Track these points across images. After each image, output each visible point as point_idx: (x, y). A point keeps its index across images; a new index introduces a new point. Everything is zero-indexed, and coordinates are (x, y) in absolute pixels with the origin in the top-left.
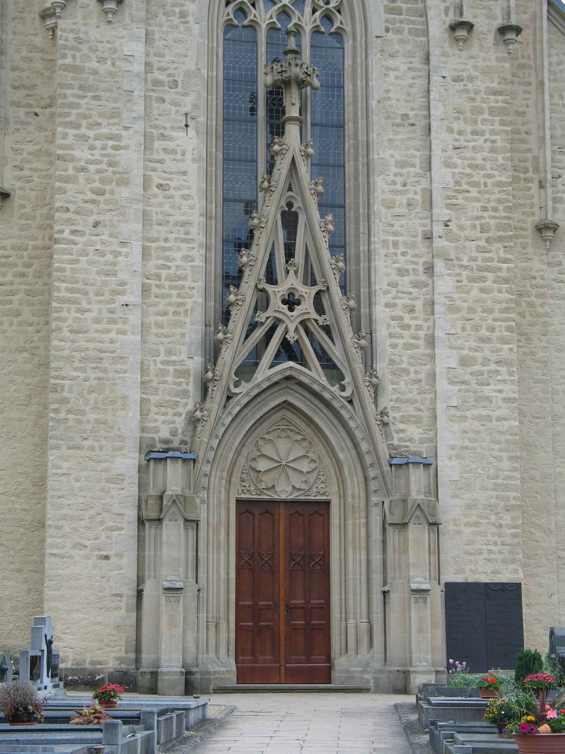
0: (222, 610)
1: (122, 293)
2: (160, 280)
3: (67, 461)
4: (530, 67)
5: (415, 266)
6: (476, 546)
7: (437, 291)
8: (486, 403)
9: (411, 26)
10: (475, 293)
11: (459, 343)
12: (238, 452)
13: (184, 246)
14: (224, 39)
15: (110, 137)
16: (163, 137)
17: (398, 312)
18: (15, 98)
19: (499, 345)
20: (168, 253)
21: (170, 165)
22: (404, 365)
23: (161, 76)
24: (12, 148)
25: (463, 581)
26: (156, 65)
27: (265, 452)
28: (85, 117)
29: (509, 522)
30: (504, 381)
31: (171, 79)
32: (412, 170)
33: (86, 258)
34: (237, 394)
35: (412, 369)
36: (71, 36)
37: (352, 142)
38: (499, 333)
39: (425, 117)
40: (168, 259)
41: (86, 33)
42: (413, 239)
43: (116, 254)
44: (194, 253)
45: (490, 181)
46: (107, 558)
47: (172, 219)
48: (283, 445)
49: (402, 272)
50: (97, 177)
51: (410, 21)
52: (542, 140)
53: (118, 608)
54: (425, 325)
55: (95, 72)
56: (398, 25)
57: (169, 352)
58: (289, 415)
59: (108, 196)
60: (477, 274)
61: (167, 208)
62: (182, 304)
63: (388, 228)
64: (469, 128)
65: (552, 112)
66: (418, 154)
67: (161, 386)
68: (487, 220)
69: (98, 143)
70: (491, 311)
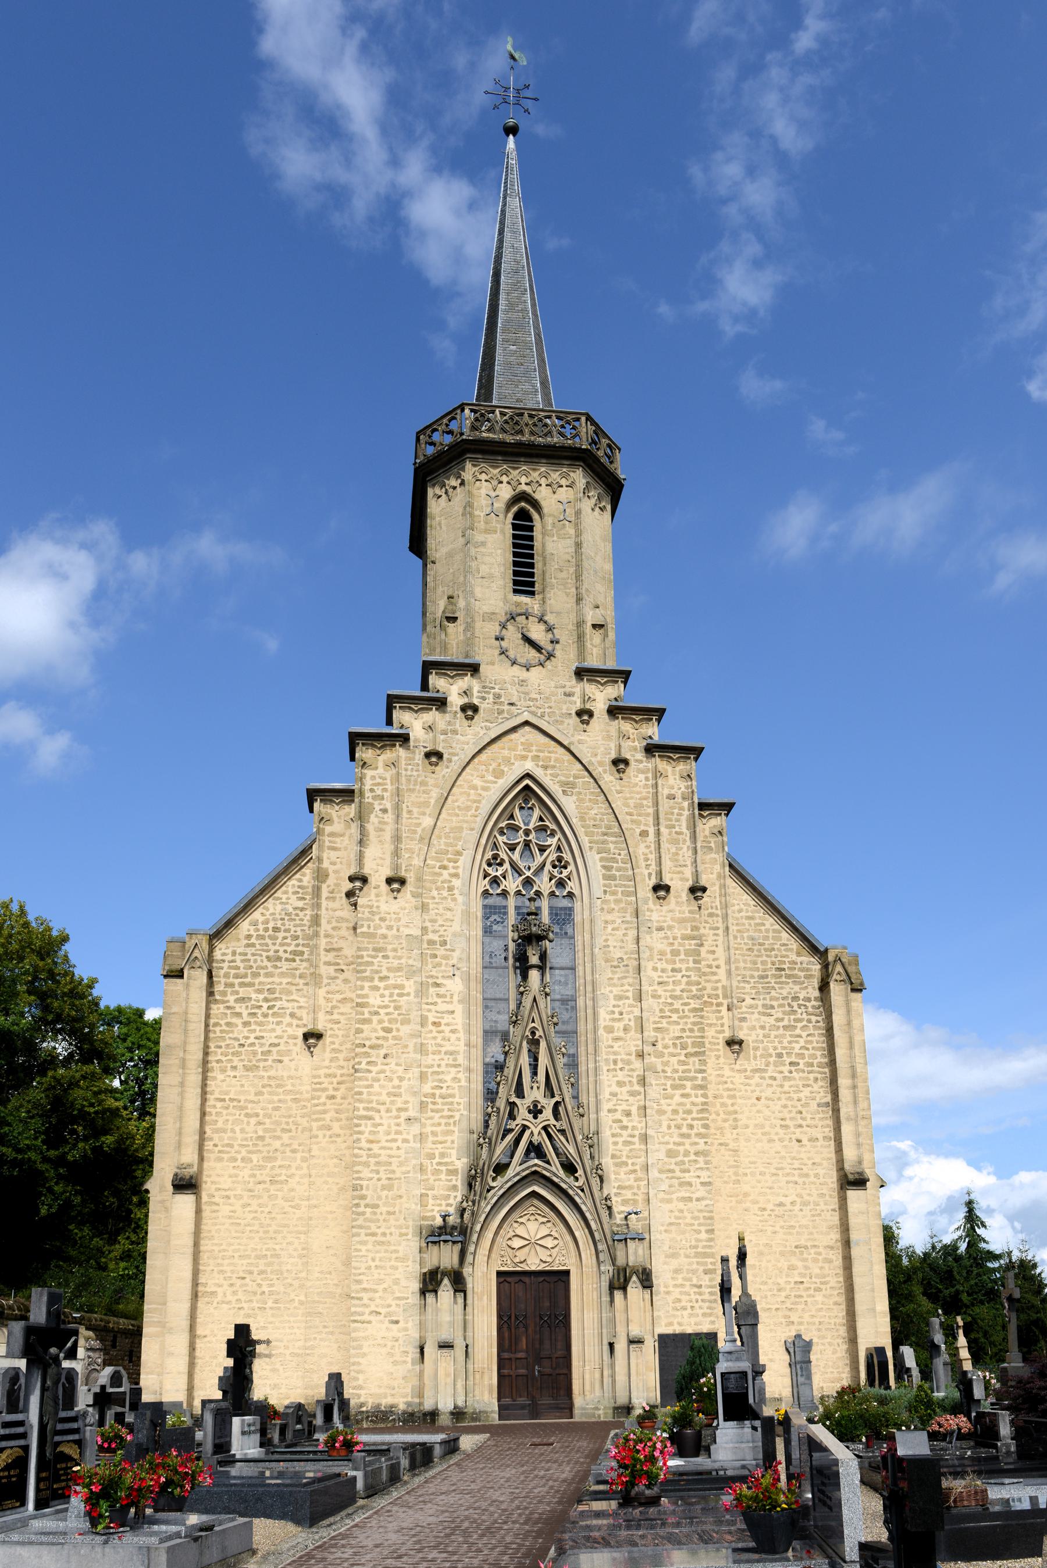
1: (406, 1110)
6: (683, 1304)
10: (677, 1099)
11: (667, 1138)
13: (453, 1070)
15: (395, 987)
16: (437, 985)
17: (618, 1116)
18: (327, 959)
19: (697, 1140)
20: (441, 1077)
22: (624, 1159)
23: (436, 938)
26: (430, 929)
27: (518, 1232)
35: (630, 1162)
40: (441, 1081)
44: (460, 1075)
45: (686, 1008)
46: (397, 1322)
47: (443, 1049)
48: (532, 1226)
49: (620, 1084)
50: (386, 1018)
53: (405, 1362)
55: (385, 937)
58: (536, 1202)
59: (394, 1033)
60: (678, 1082)
61: (439, 1041)
64: (670, 967)
69: (387, 993)
70: (689, 1112)
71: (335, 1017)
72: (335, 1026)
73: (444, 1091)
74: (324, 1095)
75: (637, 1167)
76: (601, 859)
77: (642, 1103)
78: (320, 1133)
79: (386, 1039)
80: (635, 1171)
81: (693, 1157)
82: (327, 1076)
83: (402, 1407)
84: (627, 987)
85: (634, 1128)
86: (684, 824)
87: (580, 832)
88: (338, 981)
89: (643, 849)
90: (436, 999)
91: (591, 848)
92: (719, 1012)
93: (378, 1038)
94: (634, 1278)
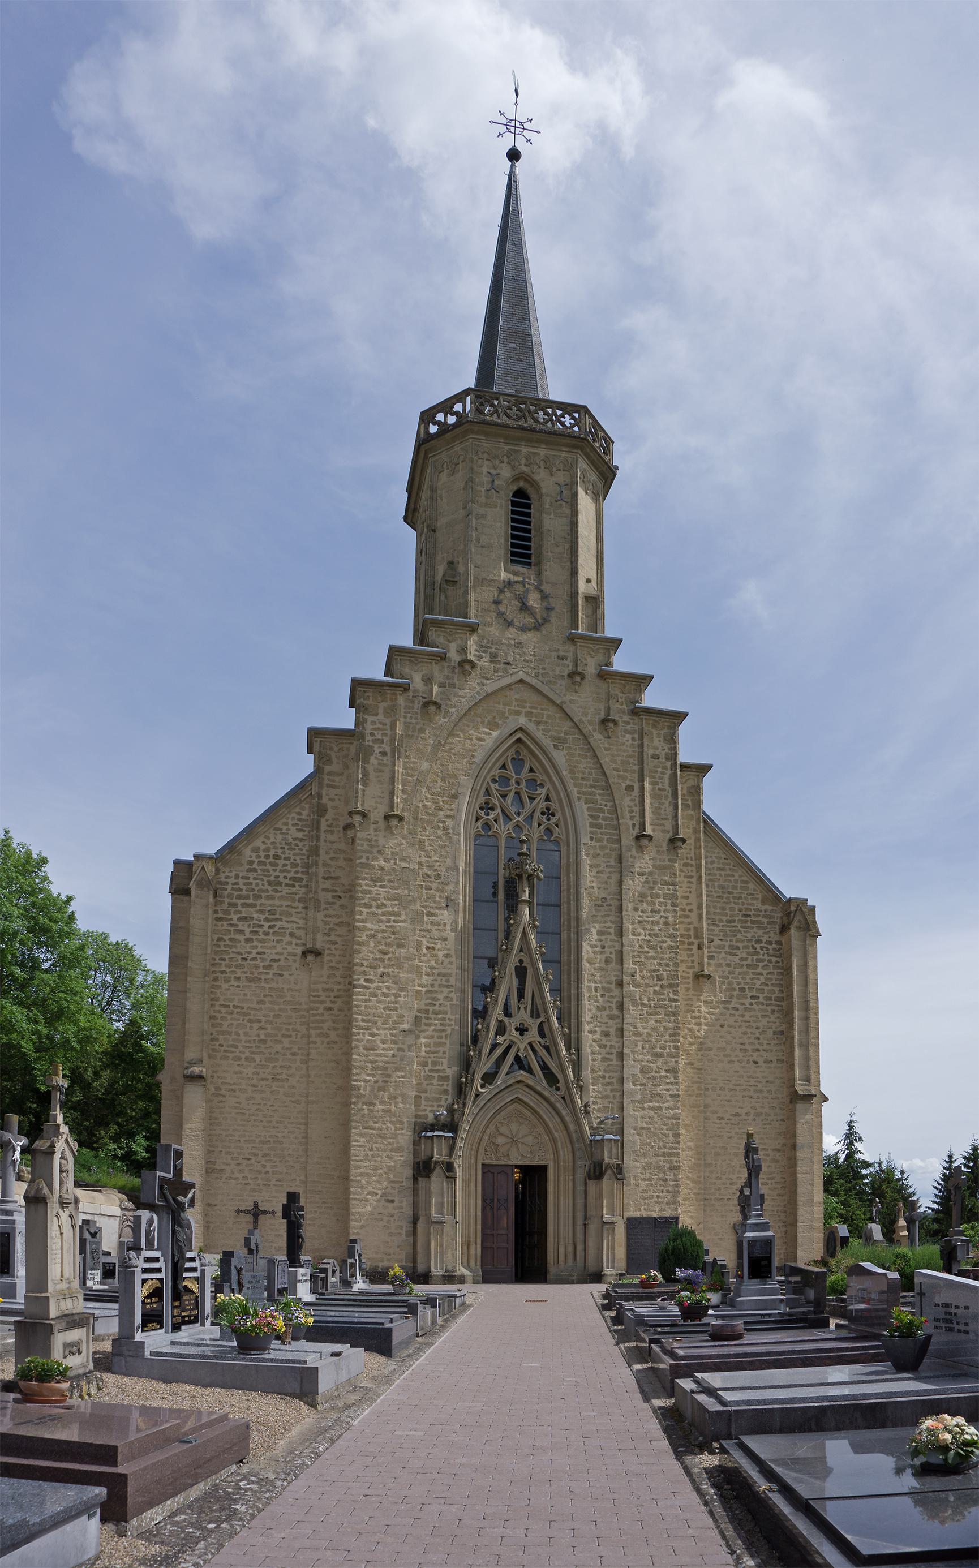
4: (692, 866)
7: (626, 1021)
13: (446, 990)
15: (394, 914)
17: (597, 1036)
18: (325, 886)
21: (436, 934)
28: (375, 900)
29: (672, 1177)
30: (671, 1083)
35: (607, 1075)
40: (434, 999)
41: (376, 841)
43: (396, 996)
46: (392, 1201)
52: (700, 916)
54: (617, 1045)
55: (382, 869)
57: (435, 1063)
65: (707, 896)
67: (429, 1087)
71: (333, 938)
72: (333, 947)
73: (437, 1008)
74: (322, 1007)
75: (614, 1080)
76: (588, 809)
77: (619, 1026)
78: (318, 1040)
79: (382, 960)
80: (611, 1083)
81: (664, 1074)
82: (324, 990)
84: (609, 924)
86: (667, 782)
88: (336, 907)
90: (429, 927)
91: (579, 799)
92: (691, 950)
93: (376, 959)
94: (609, 1172)
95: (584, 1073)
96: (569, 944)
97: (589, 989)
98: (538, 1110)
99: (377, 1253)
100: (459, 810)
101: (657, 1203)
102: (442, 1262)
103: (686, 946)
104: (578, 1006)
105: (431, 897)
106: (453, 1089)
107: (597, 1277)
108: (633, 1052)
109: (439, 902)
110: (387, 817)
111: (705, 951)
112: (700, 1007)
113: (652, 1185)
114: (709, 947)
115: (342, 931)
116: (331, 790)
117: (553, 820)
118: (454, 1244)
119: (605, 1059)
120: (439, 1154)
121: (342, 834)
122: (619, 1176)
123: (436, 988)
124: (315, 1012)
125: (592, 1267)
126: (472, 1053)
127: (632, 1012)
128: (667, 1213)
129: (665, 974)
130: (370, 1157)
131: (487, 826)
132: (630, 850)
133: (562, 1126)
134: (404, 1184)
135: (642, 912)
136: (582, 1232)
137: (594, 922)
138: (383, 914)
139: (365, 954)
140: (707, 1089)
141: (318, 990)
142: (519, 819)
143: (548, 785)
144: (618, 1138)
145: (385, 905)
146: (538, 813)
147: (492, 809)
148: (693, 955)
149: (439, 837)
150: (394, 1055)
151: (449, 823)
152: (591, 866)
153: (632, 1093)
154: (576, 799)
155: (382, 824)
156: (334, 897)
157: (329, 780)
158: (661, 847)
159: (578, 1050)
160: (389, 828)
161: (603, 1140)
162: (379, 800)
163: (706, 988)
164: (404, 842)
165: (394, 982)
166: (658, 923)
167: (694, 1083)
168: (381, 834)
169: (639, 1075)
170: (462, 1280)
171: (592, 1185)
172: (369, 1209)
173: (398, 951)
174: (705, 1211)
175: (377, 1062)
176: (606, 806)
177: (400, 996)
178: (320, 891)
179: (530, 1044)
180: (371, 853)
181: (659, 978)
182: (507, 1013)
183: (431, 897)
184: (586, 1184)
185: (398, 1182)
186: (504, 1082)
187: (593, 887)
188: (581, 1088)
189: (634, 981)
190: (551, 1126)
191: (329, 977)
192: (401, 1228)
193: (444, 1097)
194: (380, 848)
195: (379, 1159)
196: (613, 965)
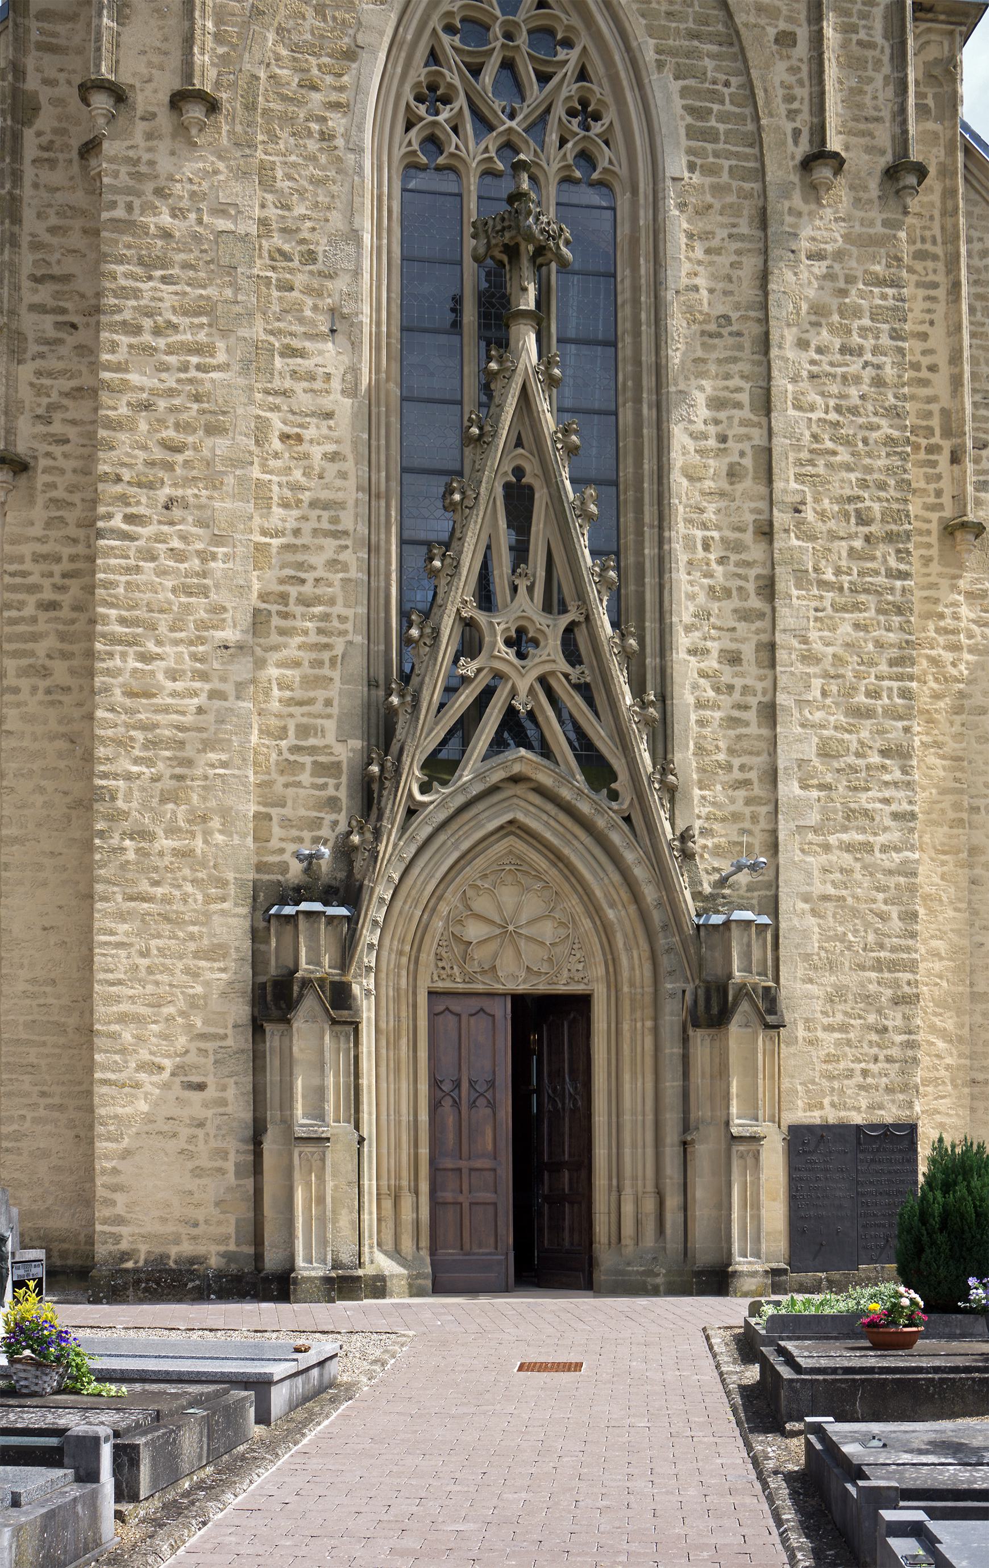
0: (405, 1174)
2: (286, 605)
3: (125, 921)
4: (935, 257)
5: (742, 583)
7: (780, 625)
8: (863, 822)
9: (734, 162)
11: (818, 716)
12: (431, 909)
13: (331, 544)
14: (404, 190)
15: (197, 350)
17: (712, 663)
18: (36, 299)
20: (300, 557)
21: (304, 401)
24: (31, 384)
25: (818, 1121)
28: (149, 314)
29: (899, 1022)
30: (895, 784)
31: (304, 248)
32: (737, 413)
33: (152, 565)
34: (425, 805)
36: (123, 170)
37: (629, 368)
38: (886, 701)
39: (759, 320)
40: (300, 566)
41: (151, 163)
42: (737, 535)
43: (205, 557)
44: (346, 556)
46: (201, 1087)
51: (732, 153)
52: (956, 382)
54: (759, 686)
55: (166, 235)
56: (711, 159)
57: (304, 731)
59: (189, 454)
62: (327, 646)
63: (694, 516)
65: (973, 335)
66: (747, 386)
67: (291, 791)
68: (868, 503)
69: (172, 360)
71: (57, 428)
72: (57, 450)
73: (308, 589)
74: (32, 600)
75: (753, 775)
76: (684, 92)
77: (765, 638)
78: (25, 683)
79: (169, 467)
80: (746, 783)
81: (875, 759)
82: (38, 558)
83: (214, 1262)
84: (736, 382)
85: (746, 690)
86: (878, 25)
87: (637, 27)
88: (64, 350)
89: (776, 75)
91: (660, 65)
92: (933, 464)
93: (152, 464)
94: (745, 1006)
95: (678, 757)
96: (638, 434)
97: (689, 543)
98: (566, 851)
99: (164, 1220)
100: (359, 89)
101: (861, 1087)
102: (323, 1242)
103: (922, 455)
104: (661, 587)
105: (293, 310)
106: (350, 796)
107: (717, 1280)
108: (800, 703)
109: (313, 323)
110: (178, 100)
111: (970, 467)
112: (955, 604)
113: (849, 1043)
114: (977, 461)
115: (77, 410)
116: (47, 58)
117: (597, 128)
118: (354, 1196)
119: (732, 722)
120: (313, 958)
121: (76, 168)
122: (770, 1019)
123: (305, 539)
124: (14, 613)
125: (704, 1255)
126: (395, 700)
127: (796, 605)
128: (889, 1115)
129: (876, 507)
130: (143, 973)
131: (433, 142)
132: (787, 195)
133: (625, 896)
134: (229, 1042)
135: (819, 351)
136: (678, 1161)
137: (700, 375)
138: (170, 350)
139: (126, 451)
140: (975, 810)
141: (21, 559)
142: (513, 124)
143: (584, 40)
144: (765, 920)
145: (175, 327)
146: (559, 111)
147: (446, 100)
148: (939, 477)
149: (313, 158)
150: (200, 711)
151: (336, 122)
152: (690, 236)
153: (799, 807)
154: (652, 66)
155: (164, 120)
156: (58, 325)
157: (42, 32)
158: (865, 189)
159: (664, 698)
160: (182, 130)
161: (727, 923)
162: (156, 59)
163: (972, 559)
164: (221, 166)
165: (200, 523)
166: (857, 380)
167: (943, 792)
168: (163, 146)
169: (816, 762)
170: (378, 1287)
171: (701, 1041)
172: (143, 1106)
173: (209, 442)
174: (973, 1110)
175: (156, 726)
176: (727, 84)
177: (214, 557)
178: (23, 310)
179: (542, 680)
180: (139, 194)
181: (863, 519)
182: (485, 598)
183: (293, 310)
184: (685, 1040)
185: (214, 1037)
186: (479, 776)
187: (696, 289)
188: (671, 792)
189: (799, 524)
190: (599, 893)
191: (49, 524)
192: (224, 1154)
193: (329, 817)
194: (162, 182)
195: (164, 978)
196: (748, 484)
